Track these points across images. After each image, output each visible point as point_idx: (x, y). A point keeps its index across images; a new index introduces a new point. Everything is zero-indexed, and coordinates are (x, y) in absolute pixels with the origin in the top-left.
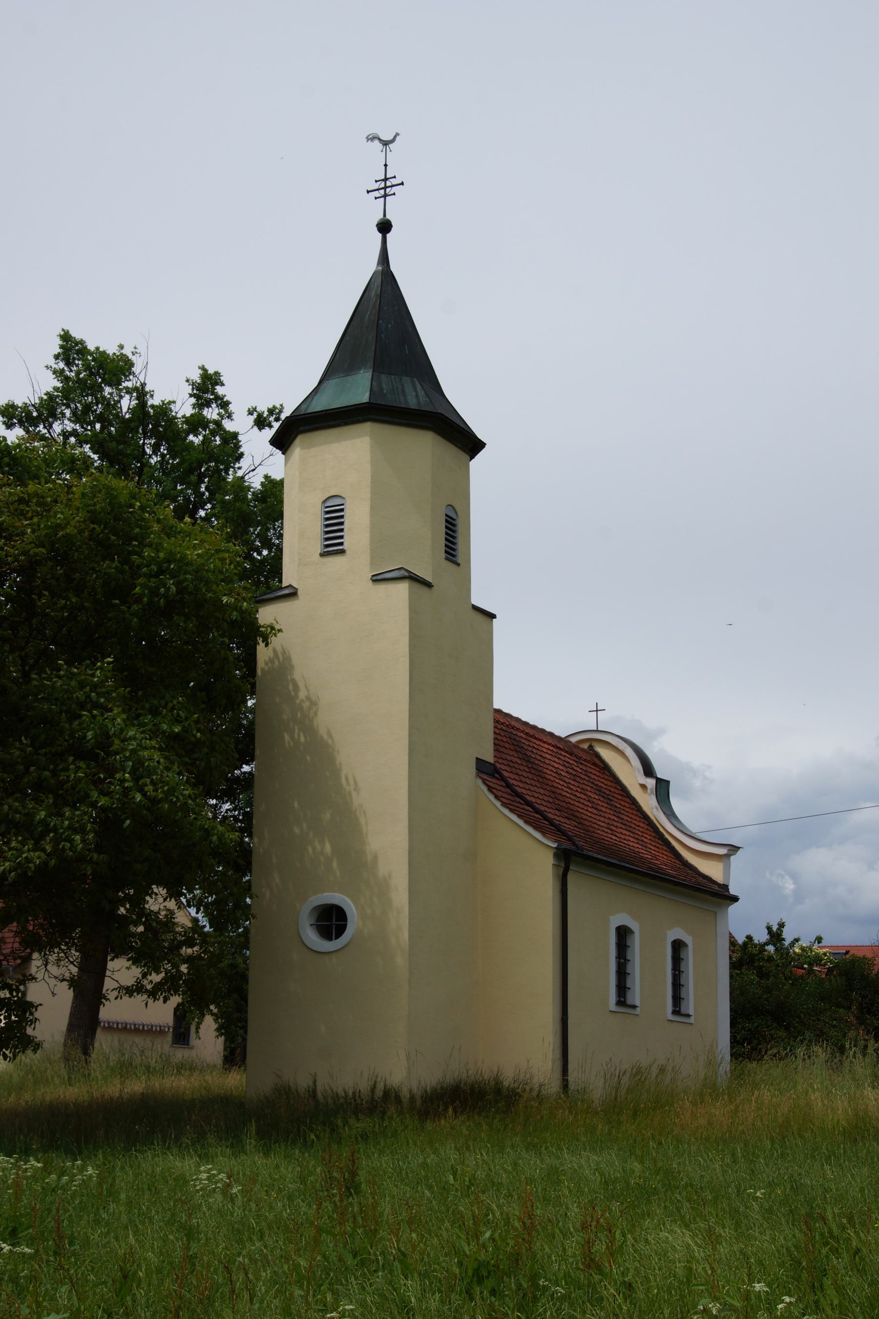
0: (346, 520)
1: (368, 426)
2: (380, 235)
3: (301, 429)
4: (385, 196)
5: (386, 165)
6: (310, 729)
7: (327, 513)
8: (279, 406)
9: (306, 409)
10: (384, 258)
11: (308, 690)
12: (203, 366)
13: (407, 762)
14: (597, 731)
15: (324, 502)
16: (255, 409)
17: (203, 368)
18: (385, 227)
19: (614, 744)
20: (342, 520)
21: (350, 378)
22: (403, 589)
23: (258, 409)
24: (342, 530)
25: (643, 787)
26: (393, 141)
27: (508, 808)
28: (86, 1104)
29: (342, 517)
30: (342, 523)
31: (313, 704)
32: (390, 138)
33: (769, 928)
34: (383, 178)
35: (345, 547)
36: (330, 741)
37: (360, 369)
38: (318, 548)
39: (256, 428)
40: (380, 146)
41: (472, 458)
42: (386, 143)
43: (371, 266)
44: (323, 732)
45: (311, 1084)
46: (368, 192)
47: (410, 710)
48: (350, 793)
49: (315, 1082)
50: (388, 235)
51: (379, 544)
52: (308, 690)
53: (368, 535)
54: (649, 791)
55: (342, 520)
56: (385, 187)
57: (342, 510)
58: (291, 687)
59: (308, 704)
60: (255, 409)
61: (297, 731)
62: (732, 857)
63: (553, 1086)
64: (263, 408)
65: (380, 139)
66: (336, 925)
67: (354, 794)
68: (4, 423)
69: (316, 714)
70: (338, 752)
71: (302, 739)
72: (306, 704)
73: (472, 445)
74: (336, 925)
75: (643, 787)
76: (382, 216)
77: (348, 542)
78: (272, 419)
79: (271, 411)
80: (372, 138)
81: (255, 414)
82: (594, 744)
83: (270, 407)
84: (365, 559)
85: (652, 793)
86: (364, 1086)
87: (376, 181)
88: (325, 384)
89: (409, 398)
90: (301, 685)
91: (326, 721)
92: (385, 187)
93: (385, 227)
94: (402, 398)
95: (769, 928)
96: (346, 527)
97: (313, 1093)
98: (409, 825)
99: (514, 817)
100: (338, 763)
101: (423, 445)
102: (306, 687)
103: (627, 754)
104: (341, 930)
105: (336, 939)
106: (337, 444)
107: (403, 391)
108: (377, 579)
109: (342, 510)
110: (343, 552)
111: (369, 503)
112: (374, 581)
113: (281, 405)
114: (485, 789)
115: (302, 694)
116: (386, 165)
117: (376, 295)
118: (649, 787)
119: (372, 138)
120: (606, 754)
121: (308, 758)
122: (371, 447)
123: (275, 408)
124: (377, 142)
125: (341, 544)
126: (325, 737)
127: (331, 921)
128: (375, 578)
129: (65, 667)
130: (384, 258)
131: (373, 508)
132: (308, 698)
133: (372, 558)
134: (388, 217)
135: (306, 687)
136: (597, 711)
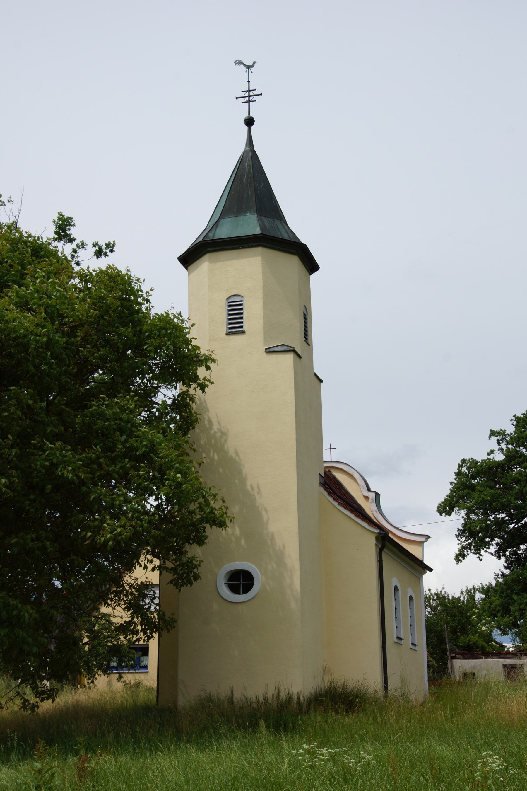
0: (245, 311)
1: (260, 249)
2: (247, 127)
3: (208, 249)
4: (249, 101)
5: (249, 82)
6: (220, 449)
7: (230, 306)
8: (112, 242)
9: (213, 237)
10: (250, 142)
11: (220, 425)
12: (61, 213)
13: (296, 474)
14: (331, 461)
15: (228, 299)
16: (97, 244)
17: (61, 214)
18: (249, 122)
19: (346, 470)
20: (241, 311)
21: (241, 218)
22: (290, 358)
23: (99, 244)
24: (242, 318)
25: (367, 498)
26: (252, 66)
27: (343, 506)
28: (368, 696)
29: (242, 309)
30: (242, 314)
31: (224, 434)
32: (251, 64)
35: (245, 329)
36: (237, 458)
37: (246, 212)
38: (224, 329)
39: (95, 257)
41: (311, 275)
42: (248, 67)
43: (241, 147)
44: (232, 453)
45: (229, 693)
47: (297, 439)
48: (254, 495)
49: (232, 692)
50: (252, 127)
51: (269, 327)
52: (220, 425)
53: (262, 321)
54: (370, 500)
55: (241, 311)
56: (249, 96)
57: (241, 305)
58: (206, 422)
59: (219, 434)
60: (97, 244)
61: (212, 452)
62: (425, 543)
63: (381, 693)
64: (102, 243)
66: (243, 584)
67: (257, 496)
69: (226, 441)
70: (244, 466)
71: (216, 457)
72: (218, 435)
73: (312, 266)
74: (243, 584)
75: (367, 498)
77: (246, 326)
78: (108, 251)
79: (107, 246)
81: (97, 248)
82: (331, 470)
83: (107, 242)
84: (261, 337)
85: (373, 501)
86: (271, 694)
87: (242, 92)
88: (222, 221)
89: (283, 233)
90: (214, 420)
91: (232, 445)
92: (249, 96)
93: (249, 122)
94: (279, 233)
96: (245, 316)
97: (231, 701)
98: (298, 516)
99: (348, 513)
100: (244, 473)
101: (293, 263)
102: (219, 422)
103: (355, 477)
104: (248, 588)
105: (244, 593)
106: (237, 261)
107: (278, 229)
108: (268, 351)
109: (241, 305)
110: (243, 332)
111: (262, 300)
112: (266, 352)
113: (114, 242)
114: (326, 494)
115: (216, 427)
116: (249, 82)
117: (249, 165)
118: (371, 498)
119: (239, 63)
120: (339, 476)
121: (221, 470)
122: (262, 263)
123: (110, 243)
124: (242, 66)
125: (242, 327)
126: (234, 455)
127: (241, 581)
128: (268, 350)
129: (107, 399)
130: (250, 142)
131: (264, 304)
132: (220, 430)
133: (265, 337)
134: (251, 115)
135: (219, 422)
136: (331, 449)
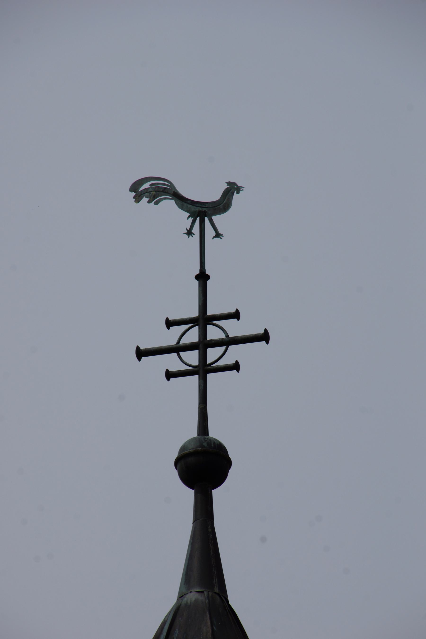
2: (189, 495)
4: (203, 370)
5: (203, 277)
17: (226, 183)
18: (204, 466)
26: (223, 205)
32: (213, 195)
33: (194, 234)
34: (195, 313)
40: (183, 219)
42: (201, 212)
46: (141, 354)
56: (203, 345)
65: (182, 201)
68: (238, 193)
76: (191, 432)
80: (153, 190)
92: (203, 345)
93: (204, 466)
95: (194, 234)
116: (203, 277)
119: (153, 190)
